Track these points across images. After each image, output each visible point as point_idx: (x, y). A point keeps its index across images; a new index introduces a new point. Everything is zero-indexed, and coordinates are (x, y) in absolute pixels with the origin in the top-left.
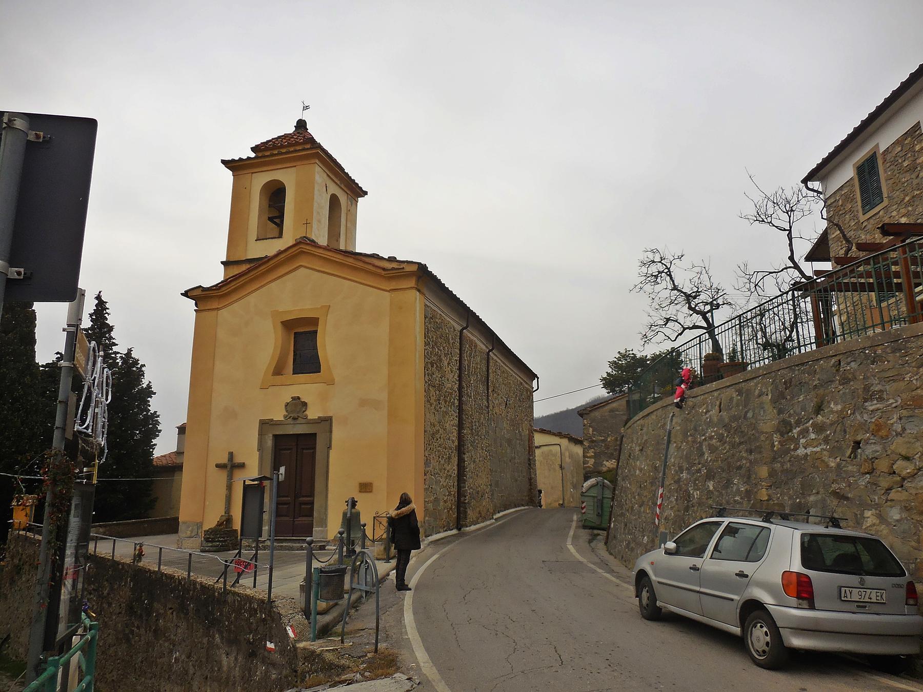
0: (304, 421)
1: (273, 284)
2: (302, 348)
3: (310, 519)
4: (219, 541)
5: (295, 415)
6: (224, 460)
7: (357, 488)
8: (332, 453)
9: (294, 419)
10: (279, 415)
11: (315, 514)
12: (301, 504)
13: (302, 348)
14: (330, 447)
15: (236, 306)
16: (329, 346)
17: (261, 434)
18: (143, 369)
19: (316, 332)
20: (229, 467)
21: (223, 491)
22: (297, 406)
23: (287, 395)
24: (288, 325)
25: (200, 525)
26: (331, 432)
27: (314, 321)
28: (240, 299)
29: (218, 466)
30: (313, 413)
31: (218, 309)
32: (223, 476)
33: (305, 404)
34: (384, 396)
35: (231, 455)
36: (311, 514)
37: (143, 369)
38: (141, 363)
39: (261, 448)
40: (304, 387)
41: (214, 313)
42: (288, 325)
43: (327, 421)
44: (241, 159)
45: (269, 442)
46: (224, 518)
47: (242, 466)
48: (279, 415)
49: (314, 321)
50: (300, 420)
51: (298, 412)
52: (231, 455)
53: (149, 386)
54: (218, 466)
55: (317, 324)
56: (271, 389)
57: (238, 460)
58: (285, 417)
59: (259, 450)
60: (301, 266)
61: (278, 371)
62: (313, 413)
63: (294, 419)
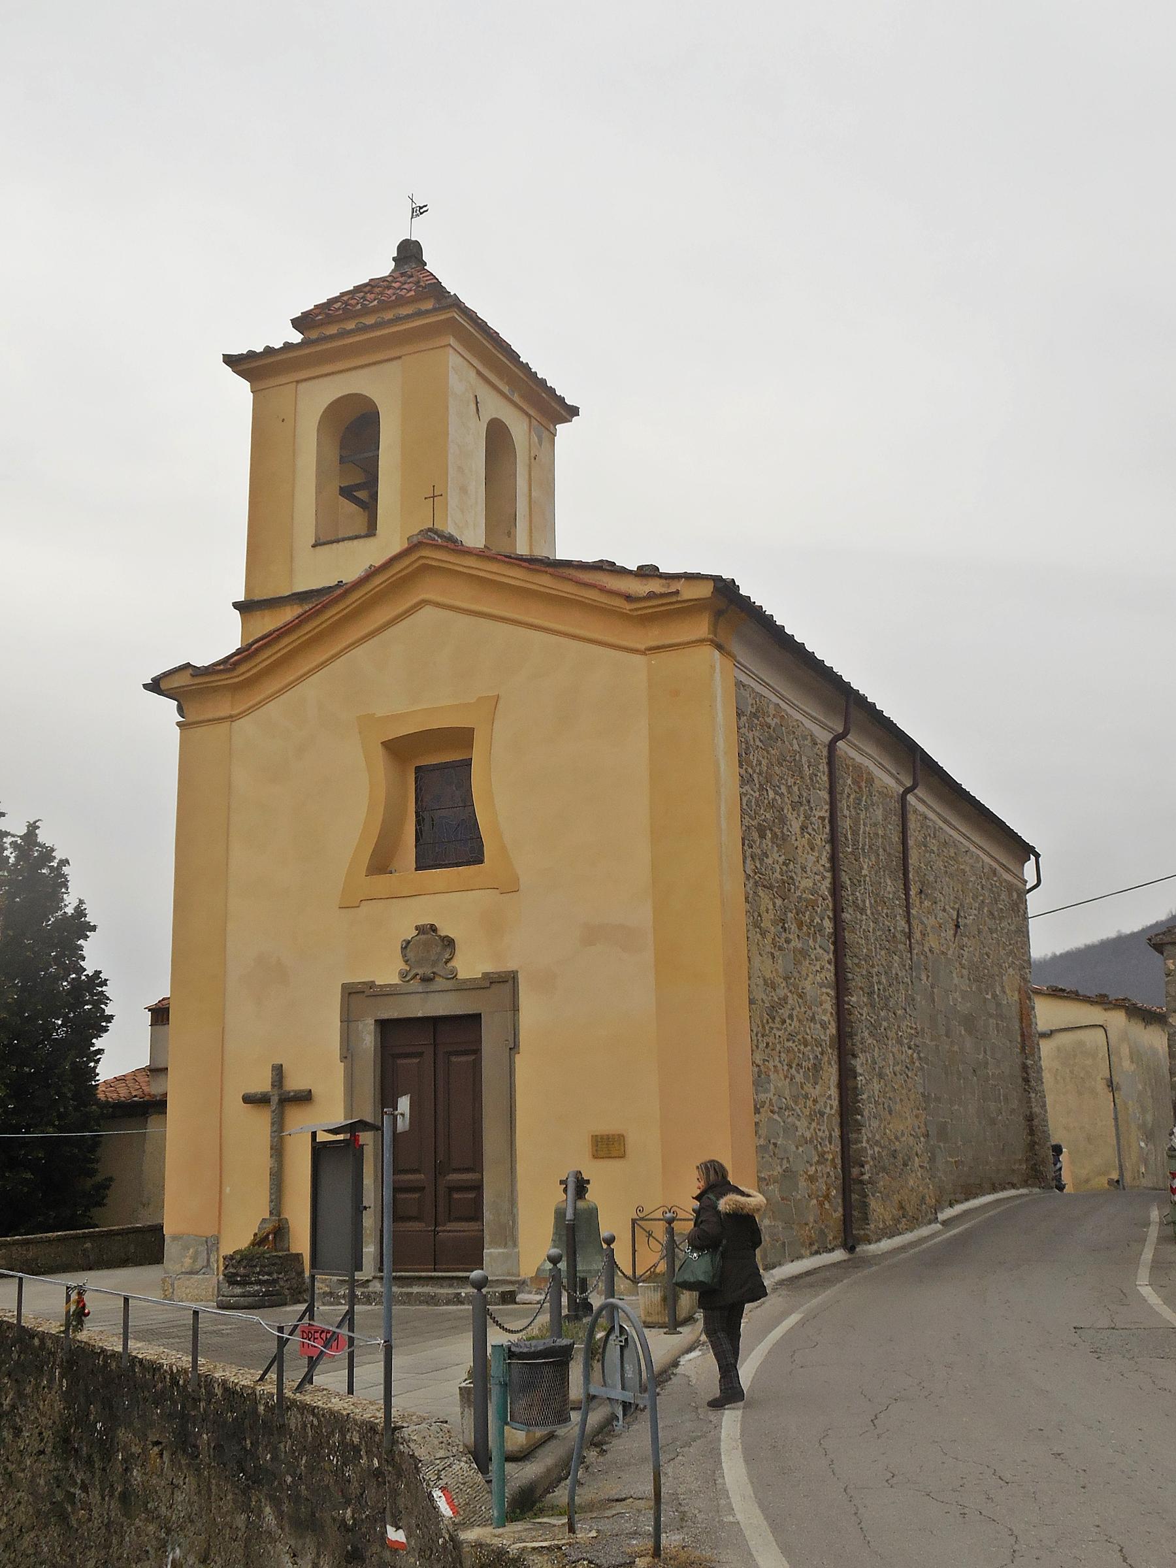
0: (449, 985)
2: (438, 808)
3: (473, 1226)
4: (259, 1282)
5: (426, 971)
6: (262, 1084)
9: (426, 980)
10: (387, 971)
11: (488, 1215)
12: (452, 1189)
13: (438, 808)
14: (514, 1048)
15: (273, 709)
16: (499, 799)
17: (348, 1020)
18: (66, 870)
19: (468, 763)
20: (275, 1100)
21: (264, 1161)
22: (431, 948)
23: (404, 922)
24: (398, 749)
25: (212, 1243)
26: (515, 1009)
29: (248, 1099)
30: (470, 964)
31: (232, 718)
32: (260, 1122)
33: (449, 943)
36: (476, 1214)
37: (66, 870)
38: (59, 855)
39: (348, 1053)
40: (447, 901)
42: (398, 749)
43: (504, 983)
44: (269, 351)
45: (368, 1038)
46: (269, 1227)
47: (305, 1098)
48: (387, 971)
49: (463, 737)
50: (440, 983)
51: (434, 963)
53: (80, 912)
54: (248, 1099)
57: (295, 1083)
58: (403, 975)
59: (344, 1058)
60: (424, 602)
61: (380, 864)
62: (470, 964)
63: (426, 980)
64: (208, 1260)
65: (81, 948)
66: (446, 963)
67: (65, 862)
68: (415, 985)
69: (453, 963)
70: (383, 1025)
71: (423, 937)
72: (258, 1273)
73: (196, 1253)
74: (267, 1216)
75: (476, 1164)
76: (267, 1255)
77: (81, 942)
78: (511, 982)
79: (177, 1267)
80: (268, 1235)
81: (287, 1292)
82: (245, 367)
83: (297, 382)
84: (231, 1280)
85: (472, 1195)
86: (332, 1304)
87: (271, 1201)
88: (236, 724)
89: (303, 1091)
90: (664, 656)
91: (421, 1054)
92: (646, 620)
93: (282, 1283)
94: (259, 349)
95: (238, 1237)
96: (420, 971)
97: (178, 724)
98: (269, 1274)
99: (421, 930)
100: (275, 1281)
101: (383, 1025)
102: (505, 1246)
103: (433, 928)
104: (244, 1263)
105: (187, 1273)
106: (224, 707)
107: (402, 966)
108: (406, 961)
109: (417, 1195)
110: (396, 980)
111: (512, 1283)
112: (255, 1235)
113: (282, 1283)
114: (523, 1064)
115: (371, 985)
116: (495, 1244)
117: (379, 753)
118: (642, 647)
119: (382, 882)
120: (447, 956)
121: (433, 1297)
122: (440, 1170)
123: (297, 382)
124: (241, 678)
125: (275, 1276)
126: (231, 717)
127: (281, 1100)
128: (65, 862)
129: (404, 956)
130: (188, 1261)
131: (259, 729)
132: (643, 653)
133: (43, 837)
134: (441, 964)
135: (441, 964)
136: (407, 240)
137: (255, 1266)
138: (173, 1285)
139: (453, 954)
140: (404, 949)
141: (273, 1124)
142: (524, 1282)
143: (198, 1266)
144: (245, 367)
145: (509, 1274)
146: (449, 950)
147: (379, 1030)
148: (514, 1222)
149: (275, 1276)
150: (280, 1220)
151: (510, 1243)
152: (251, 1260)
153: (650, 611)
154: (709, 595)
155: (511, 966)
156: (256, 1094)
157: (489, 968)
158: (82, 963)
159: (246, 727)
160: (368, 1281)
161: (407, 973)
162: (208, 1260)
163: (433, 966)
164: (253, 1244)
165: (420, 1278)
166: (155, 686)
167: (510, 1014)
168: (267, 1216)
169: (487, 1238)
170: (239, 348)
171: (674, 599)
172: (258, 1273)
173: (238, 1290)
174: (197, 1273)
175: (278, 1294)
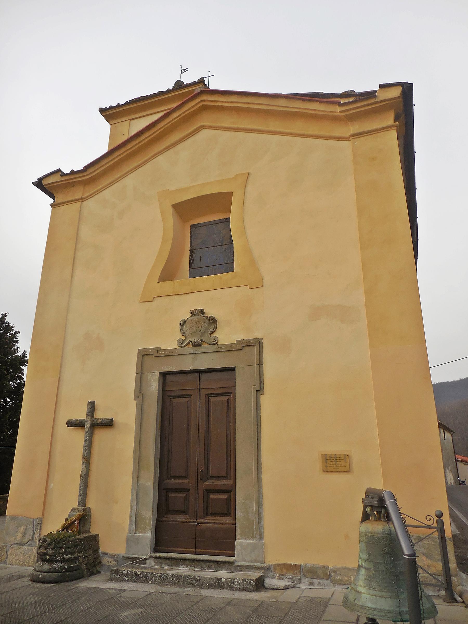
0: (213, 348)
1: (160, 158)
2: (206, 240)
3: (227, 520)
4: (63, 560)
6: (81, 414)
7: (318, 466)
8: (265, 400)
9: (196, 345)
11: (239, 513)
12: (209, 491)
13: (206, 240)
14: (260, 391)
15: (107, 193)
16: (249, 230)
17: (141, 373)
18: (17, 335)
20: (88, 425)
21: (79, 467)
22: (204, 322)
23: (183, 309)
24: (182, 209)
25: (38, 523)
26: (261, 364)
27: (222, 200)
28: (113, 183)
29: (70, 424)
30: (226, 336)
31: (82, 200)
33: (213, 321)
34: (358, 298)
35: (92, 406)
36: (228, 509)
37: (17, 335)
38: (15, 329)
39: (140, 394)
40: (214, 296)
41: (78, 204)
42: (182, 209)
44: (119, 106)
45: (154, 385)
46: (76, 515)
48: (170, 342)
49: (222, 200)
50: (205, 348)
51: (202, 334)
52: (92, 406)
53: (24, 355)
54: (70, 424)
55: (228, 209)
56: (158, 301)
57: (100, 415)
58: (181, 343)
59: (136, 398)
60: (203, 127)
61: (167, 275)
62: (226, 336)
64: (33, 536)
65: (23, 370)
66: (211, 334)
67: (18, 332)
68: (189, 349)
69: (215, 334)
70: (164, 375)
71: (195, 317)
72: (63, 553)
73: (26, 530)
74: (76, 506)
75: (229, 472)
76: (71, 539)
77: (23, 368)
78: (257, 346)
79: (12, 540)
80: (74, 522)
81: (84, 567)
82: (106, 114)
83: (131, 120)
84: (42, 557)
85: (225, 496)
86: (117, 580)
87: (80, 496)
88: (85, 203)
89: (107, 419)
90: (362, 139)
91: (190, 396)
92: (351, 118)
93: (81, 560)
94: (114, 105)
95: (53, 526)
96: (192, 340)
97: (51, 205)
98: (71, 554)
99: (193, 313)
100: (76, 559)
101: (164, 375)
102: (253, 538)
103: (202, 312)
104: (52, 546)
105: (17, 544)
106: (78, 193)
107: (179, 336)
108: (183, 334)
109: (184, 495)
110: (174, 346)
111: (259, 568)
112: (66, 520)
113: (81, 560)
114: (266, 401)
115: (158, 350)
116: (245, 536)
117: (170, 212)
118: (348, 135)
119: (168, 286)
120: (211, 330)
121: (198, 581)
122: (204, 476)
123: (131, 120)
124: (90, 176)
125: (76, 555)
126: (82, 198)
127: (94, 424)
128: (18, 332)
129: (182, 330)
130: (19, 535)
131: (99, 205)
132: (348, 139)
133: (8, 320)
134: (207, 335)
135: (207, 335)
136: (179, 80)
137: (61, 548)
138: (7, 552)
139: (215, 328)
140: (182, 326)
141: (85, 441)
142: (268, 569)
143: (26, 540)
144: (106, 114)
145: (256, 561)
146: (212, 326)
147: (162, 380)
148: (260, 518)
149: (76, 555)
150: (84, 510)
151: (257, 536)
152: (59, 543)
153: (354, 111)
154: (399, 95)
155: (257, 335)
156: (75, 421)
157: (242, 337)
158: (22, 376)
159: (90, 204)
160: (145, 559)
161: (183, 341)
162: (33, 536)
163: (201, 336)
164: (65, 528)
165: (185, 560)
166: (39, 184)
167: (256, 368)
168: (76, 506)
169: (238, 531)
170: (106, 105)
171: (372, 101)
172: (63, 553)
173: (46, 567)
174: (24, 544)
175: (78, 568)
